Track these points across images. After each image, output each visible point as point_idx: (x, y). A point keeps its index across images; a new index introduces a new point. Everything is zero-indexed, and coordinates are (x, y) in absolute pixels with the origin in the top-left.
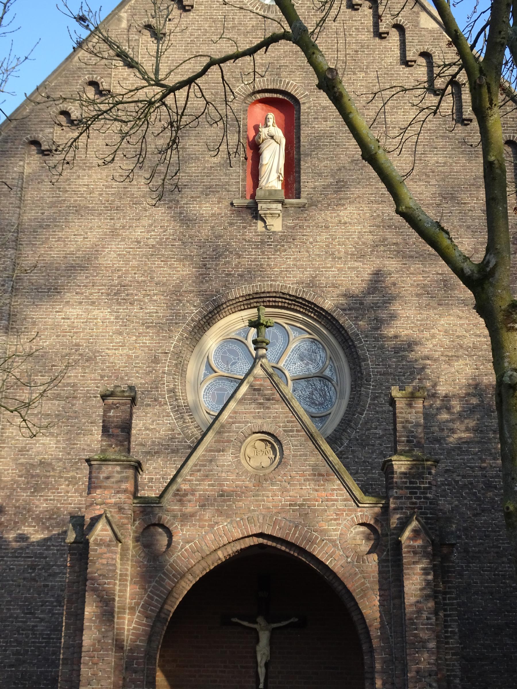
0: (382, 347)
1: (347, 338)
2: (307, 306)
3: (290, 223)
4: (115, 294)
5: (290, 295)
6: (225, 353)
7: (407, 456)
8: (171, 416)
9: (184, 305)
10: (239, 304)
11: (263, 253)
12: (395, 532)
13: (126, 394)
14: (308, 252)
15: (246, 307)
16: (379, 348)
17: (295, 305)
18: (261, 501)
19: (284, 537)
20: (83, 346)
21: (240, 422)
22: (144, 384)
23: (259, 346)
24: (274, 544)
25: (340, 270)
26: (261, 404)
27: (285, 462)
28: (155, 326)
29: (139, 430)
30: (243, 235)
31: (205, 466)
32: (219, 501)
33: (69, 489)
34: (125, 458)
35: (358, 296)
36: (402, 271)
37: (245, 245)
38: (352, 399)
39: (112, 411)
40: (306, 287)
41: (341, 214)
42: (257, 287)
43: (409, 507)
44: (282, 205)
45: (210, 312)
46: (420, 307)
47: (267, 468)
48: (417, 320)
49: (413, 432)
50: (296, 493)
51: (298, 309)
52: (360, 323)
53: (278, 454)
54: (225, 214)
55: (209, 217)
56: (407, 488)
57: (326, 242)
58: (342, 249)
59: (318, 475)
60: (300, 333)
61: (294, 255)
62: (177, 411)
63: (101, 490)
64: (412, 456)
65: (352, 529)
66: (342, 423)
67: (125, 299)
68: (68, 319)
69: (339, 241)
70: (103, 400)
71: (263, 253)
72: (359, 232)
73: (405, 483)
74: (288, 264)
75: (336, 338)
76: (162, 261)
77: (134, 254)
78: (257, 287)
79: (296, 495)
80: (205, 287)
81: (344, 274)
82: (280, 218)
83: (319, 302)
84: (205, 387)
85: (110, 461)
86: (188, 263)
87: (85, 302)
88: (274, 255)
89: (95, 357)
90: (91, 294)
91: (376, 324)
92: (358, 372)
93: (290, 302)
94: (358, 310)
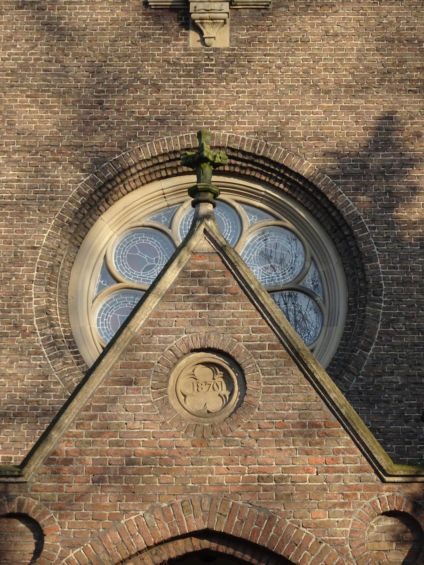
0: (398, 239)
1: (341, 223)
2: (273, 171)
3: (243, 35)
5: (244, 153)
6: (133, 250)
8: (42, 353)
9: (65, 169)
10: (157, 168)
11: (198, 83)
14: (273, 81)
15: (170, 173)
17: (252, 169)
18: (206, 473)
19: (249, 537)
21: (166, 332)
23: (200, 198)
24: (230, 551)
25: (327, 111)
27: (249, 403)
28: (16, 204)
30: (164, 53)
31: (103, 409)
32: (130, 472)
35: (358, 154)
37: (167, 70)
38: (349, 325)
40: (272, 139)
41: (329, 20)
42: (188, 140)
44: (231, 5)
45: (110, 181)
47: (216, 414)
50: (270, 457)
51: (258, 176)
53: (237, 388)
54: (135, 20)
55: (107, 24)
57: (303, 65)
58: (331, 77)
59: (307, 430)
60: (260, 218)
61: (251, 86)
62: (53, 344)
65: (372, 523)
66: (334, 365)
69: (325, 65)
71: (198, 83)
72: (359, 50)
74: (241, 102)
76: (27, 96)
78: (188, 140)
79: (269, 461)
80: (98, 139)
81: (335, 118)
82: (227, 27)
83: (294, 163)
84: (101, 306)
86: (71, 99)
88: (216, 86)
91: (389, 200)
92: (360, 280)
93: (244, 165)
94: (359, 178)
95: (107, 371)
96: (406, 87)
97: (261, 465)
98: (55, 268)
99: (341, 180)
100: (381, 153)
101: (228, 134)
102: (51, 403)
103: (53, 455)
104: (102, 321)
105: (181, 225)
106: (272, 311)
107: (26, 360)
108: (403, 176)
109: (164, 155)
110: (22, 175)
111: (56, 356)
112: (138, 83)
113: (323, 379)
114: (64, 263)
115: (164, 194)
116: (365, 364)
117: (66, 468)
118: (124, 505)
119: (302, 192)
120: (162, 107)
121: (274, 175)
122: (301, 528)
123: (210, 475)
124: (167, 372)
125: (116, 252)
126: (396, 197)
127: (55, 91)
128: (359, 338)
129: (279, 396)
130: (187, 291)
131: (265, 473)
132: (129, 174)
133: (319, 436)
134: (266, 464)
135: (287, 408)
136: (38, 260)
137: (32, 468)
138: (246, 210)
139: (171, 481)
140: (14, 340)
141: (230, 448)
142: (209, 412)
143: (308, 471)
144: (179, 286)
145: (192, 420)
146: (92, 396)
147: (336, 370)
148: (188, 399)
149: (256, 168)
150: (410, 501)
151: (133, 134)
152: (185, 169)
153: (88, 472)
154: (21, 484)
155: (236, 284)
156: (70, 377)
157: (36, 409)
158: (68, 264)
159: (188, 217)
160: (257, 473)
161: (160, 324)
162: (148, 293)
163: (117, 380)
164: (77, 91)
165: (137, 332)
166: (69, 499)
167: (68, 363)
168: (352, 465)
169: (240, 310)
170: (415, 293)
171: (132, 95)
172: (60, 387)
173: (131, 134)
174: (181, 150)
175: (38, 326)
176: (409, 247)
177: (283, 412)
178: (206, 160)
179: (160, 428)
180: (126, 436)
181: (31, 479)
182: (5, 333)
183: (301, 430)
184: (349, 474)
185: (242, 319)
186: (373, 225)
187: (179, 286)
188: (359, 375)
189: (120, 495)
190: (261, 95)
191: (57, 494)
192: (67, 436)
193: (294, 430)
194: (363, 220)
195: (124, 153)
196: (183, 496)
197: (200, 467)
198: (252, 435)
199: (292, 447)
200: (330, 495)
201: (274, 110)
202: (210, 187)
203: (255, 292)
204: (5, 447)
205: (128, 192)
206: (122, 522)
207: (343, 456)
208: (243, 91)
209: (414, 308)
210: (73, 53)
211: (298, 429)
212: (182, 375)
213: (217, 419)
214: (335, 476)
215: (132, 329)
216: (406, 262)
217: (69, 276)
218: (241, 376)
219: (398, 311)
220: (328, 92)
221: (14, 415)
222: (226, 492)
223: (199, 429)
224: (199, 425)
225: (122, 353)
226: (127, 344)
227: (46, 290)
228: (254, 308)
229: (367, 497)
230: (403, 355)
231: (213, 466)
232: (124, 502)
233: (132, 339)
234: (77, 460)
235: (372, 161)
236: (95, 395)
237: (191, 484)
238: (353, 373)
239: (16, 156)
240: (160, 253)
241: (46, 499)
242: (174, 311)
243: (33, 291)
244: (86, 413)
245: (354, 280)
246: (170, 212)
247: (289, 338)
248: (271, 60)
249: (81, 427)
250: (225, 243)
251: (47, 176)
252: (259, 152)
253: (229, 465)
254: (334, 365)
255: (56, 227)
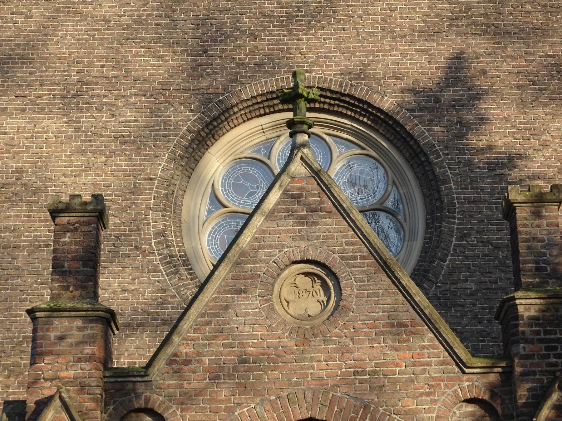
0: (469, 163)
1: (418, 150)
2: (358, 107)
4: (74, 96)
5: (332, 92)
6: (237, 179)
7: (538, 292)
9: (176, 109)
10: (257, 107)
11: (290, 32)
12: (525, 410)
13: (89, 208)
14: (356, 29)
15: (267, 111)
16: (466, 164)
17: (339, 106)
18: (308, 369)
20: (27, 172)
21: (270, 247)
22: (119, 225)
23: (297, 129)
25: (404, 54)
26: (302, 217)
27: (344, 307)
28: (134, 141)
29: (114, 293)
30: (260, 7)
31: (217, 315)
32: (242, 370)
33: (10, 383)
34: (89, 306)
35: (431, 90)
36: (495, 53)
38: (428, 240)
39: (68, 234)
40: (356, 79)
42: (283, 81)
43: (546, 371)
45: (215, 119)
46: (524, 104)
47: (316, 317)
48: (521, 123)
49: (544, 255)
50: (364, 354)
51: (344, 111)
52: (436, 129)
53: (333, 294)
56: (541, 341)
57: (382, 14)
59: (397, 328)
60: (348, 148)
61: (336, 34)
63: (53, 357)
64: (546, 291)
66: (415, 275)
67: (88, 103)
68: (5, 133)
70: (54, 219)
71: (290, 32)
73: (537, 333)
74: (328, 48)
75: (401, 152)
76: (141, 47)
77: (101, 39)
78: (283, 81)
79: (363, 357)
80: (205, 83)
81: (410, 59)
83: (375, 100)
84: (210, 229)
85: (65, 310)
86: (179, 49)
87: (30, 109)
88: (306, 34)
89: (46, 188)
90: (38, 97)
92: (436, 200)
93: (332, 102)
94: (433, 111)
95: (219, 282)
96: (472, 31)
97: (358, 360)
98: (169, 196)
99: (417, 114)
100: (451, 89)
101: (317, 76)
102: (169, 314)
103: (174, 357)
104: (212, 241)
105: (279, 156)
106: (362, 226)
107: (146, 277)
108: (471, 109)
109: (261, 95)
110: (138, 116)
111: (172, 273)
112: (238, 33)
113: (408, 284)
114: (177, 192)
115: (263, 129)
116: (443, 273)
117: (186, 368)
118: (237, 398)
119: (384, 124)
120: (259, 54)
121: (358, 110)
122: (393, 415)
123: (312, 371)
124: (272, 282)
125: (222, 181)
126: (465, 127)
127: (165, 43)
128: (436, 251)
129: (370, 300)
130: (288, 210)
131: (360, 367)
132: (232, 113)
133: (406, 335)
134: (361, 360)
135: (377, 310)
136: (155, 189)
137: (156, 369)
138: (335, 141)
139: (278, 377)
140: (135, 260)
141: (328, 346)
142: (309, 316)
143: (397, 365)
144: (280, 207)
145: (295, 323)
146: (207, 304)
147: (420, 276)
148: (290, 305)
149: (343, 104)
150: (487, 390)
151: (234, 78)
152: (281, 107)
153: (205, 371)
154: (147, 383)
155: (330, 203)
156: (185, 291)
157: (155, 319)
158: (180, 192)
159: (284, 148)
160: (353, 368)
161: (265, 240)
162: (251, 216)
163: (228, 290)
164: (184, 41)
165: (245, 248)
166: (189, 394)
167: (183, 279)
168: (436, 359)
169: (335, 226)
170: (485, 210)
171: (232, 43)
172: (176, 300)
173: (233, 78)
174: (277, 90)
175: (156, 247)
176: (478, 170)
177: (374, 314)
178: (301, 96)
179: (267, 331)
180: (238, 338)
181: (155, 378)
182: (127, 254)
183: (390, 329)
184: (434, 367)
185: (336, 234)
186: (447, 152)
187: (280, 207)
188: (437, 282)
189: (234, 391)
190: (345, 41)
191: (178, 391)
192: (186, 340)
193: (385, 329)
194: (438, 148)
195: (227, 95)
196: (289, 390)
197: (303, 364)
198: (348, 335)
199: (383, 344)
200: (417, 386)
201: (357, 54)
202: (305, 120)
203: (347, 210)
204: (130, 353)
205: (232, 128)
206: (236, 413)
207: (428, 351)
208: (329, 38)
209: (484, 224)
210: (180, 9)
211: (387, 329)
212: (285, 284)
213: (317, 322)
214: (422, 369)
215: (240, 245)
216: (476, 183)
217: (182, 202)
218: (336, 284)
219: (470, 226)
220: (403, 37)
221: (137, 325)
222: (326, 385)
223: (301, 331)
224: (301, 327)
225: (232, 266)
226: (236, 258)
227: (163, 216)
228: (346, 223)
229: (450, 387)
230: (476, 264)
231: (314, 363)
232: (237, 396)
233: (240, 254)
234: (195, 360)
235: (443, 96)
236: (209, 304)
237: (295, 379)
238: (432, 281)
239: (133, 100)
240: (261, 181)
241: (169, 395)
242: (277, 228)
243: (150, 216)
244: (202, 319)
245: (431, 200)
246: (269, 145)
247: (377, 249)
248: (353, 11)
249: (198, 332)
250: (319, 168)
251: (160, 117)
252: (345, 90)
253: (328, 361)
254: (415, 275)
255: (170, 160)
